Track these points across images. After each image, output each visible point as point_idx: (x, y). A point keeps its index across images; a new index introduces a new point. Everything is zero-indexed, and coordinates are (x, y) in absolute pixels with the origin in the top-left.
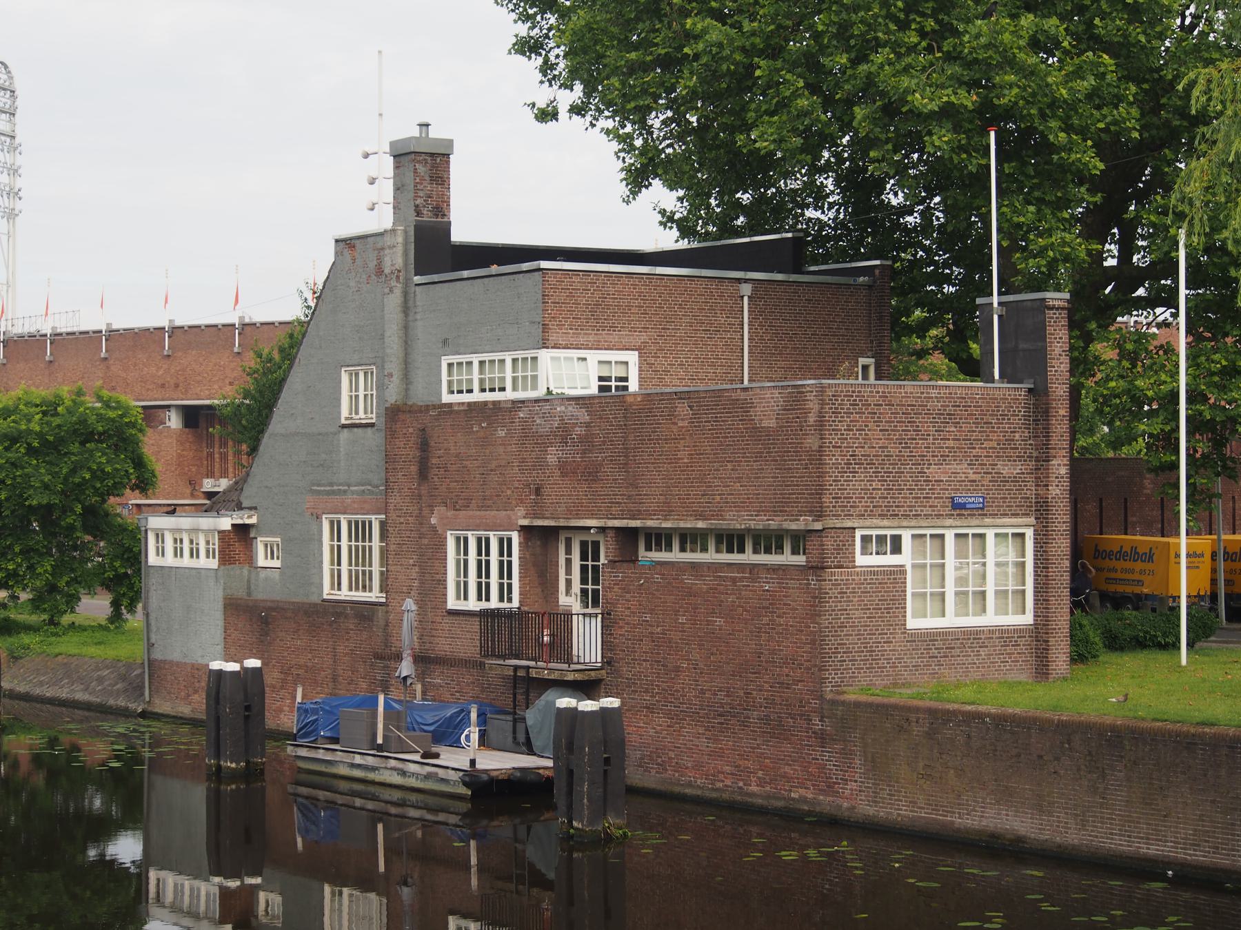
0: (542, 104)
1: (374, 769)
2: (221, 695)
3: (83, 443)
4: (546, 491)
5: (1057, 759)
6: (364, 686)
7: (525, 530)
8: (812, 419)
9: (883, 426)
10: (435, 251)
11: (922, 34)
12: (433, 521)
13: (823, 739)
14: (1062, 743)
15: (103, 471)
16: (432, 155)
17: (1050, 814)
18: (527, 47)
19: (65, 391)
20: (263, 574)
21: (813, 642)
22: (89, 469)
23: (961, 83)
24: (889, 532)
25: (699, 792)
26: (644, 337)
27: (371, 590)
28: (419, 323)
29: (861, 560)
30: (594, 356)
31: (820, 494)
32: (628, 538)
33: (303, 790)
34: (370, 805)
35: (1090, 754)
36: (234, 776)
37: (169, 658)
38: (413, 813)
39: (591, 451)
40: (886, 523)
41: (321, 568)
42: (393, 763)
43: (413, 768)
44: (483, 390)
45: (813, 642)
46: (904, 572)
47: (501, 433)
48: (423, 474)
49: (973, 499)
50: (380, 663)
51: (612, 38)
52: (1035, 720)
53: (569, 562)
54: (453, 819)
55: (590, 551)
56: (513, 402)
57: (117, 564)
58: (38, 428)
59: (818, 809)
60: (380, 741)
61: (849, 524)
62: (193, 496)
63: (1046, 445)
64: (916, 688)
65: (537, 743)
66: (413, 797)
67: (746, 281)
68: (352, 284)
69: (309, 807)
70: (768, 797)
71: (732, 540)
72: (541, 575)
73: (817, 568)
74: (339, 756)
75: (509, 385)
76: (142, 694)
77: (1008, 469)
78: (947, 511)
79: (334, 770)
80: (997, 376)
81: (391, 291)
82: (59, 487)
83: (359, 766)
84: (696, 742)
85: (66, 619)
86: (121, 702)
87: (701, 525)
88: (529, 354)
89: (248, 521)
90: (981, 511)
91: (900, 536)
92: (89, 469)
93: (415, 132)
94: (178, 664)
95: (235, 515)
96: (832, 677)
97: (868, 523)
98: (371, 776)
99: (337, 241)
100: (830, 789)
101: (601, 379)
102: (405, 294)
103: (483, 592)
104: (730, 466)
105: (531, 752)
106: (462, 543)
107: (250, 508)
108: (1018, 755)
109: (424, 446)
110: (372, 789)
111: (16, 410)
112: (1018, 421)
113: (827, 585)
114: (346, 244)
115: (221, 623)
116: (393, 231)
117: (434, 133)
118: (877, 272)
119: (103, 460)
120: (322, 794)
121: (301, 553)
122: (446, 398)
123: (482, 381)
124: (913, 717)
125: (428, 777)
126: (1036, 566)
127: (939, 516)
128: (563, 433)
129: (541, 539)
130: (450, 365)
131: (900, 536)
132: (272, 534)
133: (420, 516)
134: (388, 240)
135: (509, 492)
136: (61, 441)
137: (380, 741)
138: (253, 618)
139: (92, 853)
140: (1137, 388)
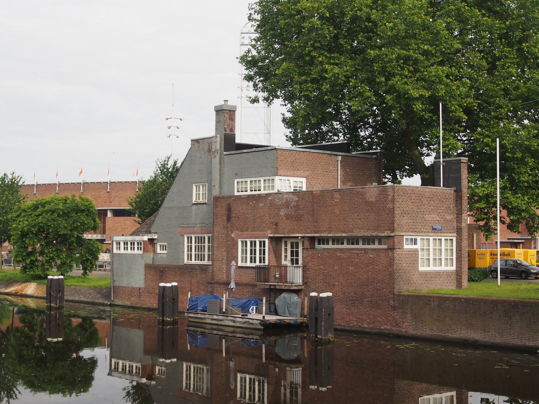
0: (253, 97)
1: (221, 320)
2: (165, 295)
3: (76, 213)
4: (279, 224)
5: (492, 313)
6: (203, 293)
7: (271, 238)
8: (390, 198)
9: (412, 201)
10: (230, 144)
11: (410, 72)
12: (233, 236)
13: (394, 308)
14: (494, 308)
15: (84, 223)
16: (230, 111)
17: (489, 332)
18: (249, 78)
19: (69, 196)
20: (159, 256)
21: (390, 275)
22: (79, 222)
23: (425, 88)
24: (413, 237)
25: (343, 328)
26: (308, 173)
27: (204, 260)
28: (226, 168)
29: (406, 247)
30: (292, 179)
31: (393, 223)
32: (312, 240)
33: (192, 329)
34: (220, 333)
35: (505, 311)
36: (169, 323)
37: (121, 285)
38: (238, 335)
39: (298, 210)
40: (413, 234)
41: (184, 253)
42: (230, 318)
43: (238, 319)
44: (251, 191)
45: (390, 275)
46: (418, 251)
47: (261, 205)
48: (229, 219)
49: (438, 227)
50: (210, 286)
51: (296, 72)
52: (482, 300)
53: (286, 250)
54: (256, 337)
55: (294, 245)
56: (266, 194)
57: (87, 255)
58: (62, 208)
59: (392, 332)
60: (224, 310)
61: (402, 234)
63: (461, 209)
64: (425, 289)
65: (279, 311)
66: (238, 330)
67: (339, 155)
68: (198, 155)
69: (193, 335)
70: (371, 328)
71: (354, 240)
72: (277, 254)
73: (392, 249)
74: (207, 316)
75: (262, 189)
76: (110, 297)
77: (449, 217)
78: (431, 230)
79: (205, 321)
80: (442, 186)
81: (215, 157)
82: (69, 228)
83: (215, 319)
84: (342, 310)
85: (69, 274)
86: (101, 301)
87: (344, 235)
88: (271, 178)
89: (154, 237)
90: (441, 231)
92: (79, 222)
93: (223, 103)
94: (125, 287)
95: (149, 235)
96: (397, 287)
97: (408, 234)
98: (220, 323)
99: (192, 140)
100: (397, 325)
101: (294, 187)
102: (220, 158)
103: (253, 260)
104: (356, 215)
105: (276, 314)
106: (245, 244)
107: (154, 233)
108: (476, 312)
109: (229, 210)
110: (221, 327)
111: (52, 201)
112: (451, 201)
113: (395, 255)
114: (195, 142)
115: (143, 273)
116: (216, 137)
117: (229, 103)
118: (379, 154)
119: (84, 219)
120: (199, 330)
121: (175, 247)
122: (236, 194)
123: (251, 188)
124: (432, 300)
125: (244, 323)
126: (457, 250)
128: (287, 204)
129: (276, 241)
130: (238, 182)
132: (163, 241)
133: (227, 234)
134: (214, 140)
135: (264, 225)
136: (69, 212)
137: (224, 310)
138: (157, 271)
139: (74, 355)
140: (476, 192)
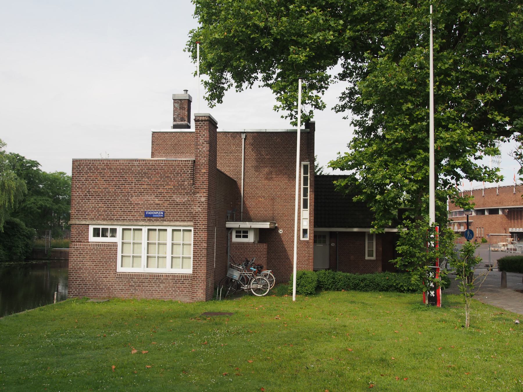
16: (180, 100)
29: (92, 239)
40: (105, 223)
49: (158, 212)
62: (506, 233)
90: (163, 218)
91: (116, 229)
127: (137, 220)
131: (116, 229)
